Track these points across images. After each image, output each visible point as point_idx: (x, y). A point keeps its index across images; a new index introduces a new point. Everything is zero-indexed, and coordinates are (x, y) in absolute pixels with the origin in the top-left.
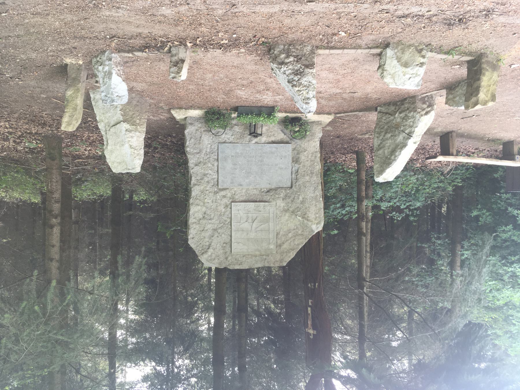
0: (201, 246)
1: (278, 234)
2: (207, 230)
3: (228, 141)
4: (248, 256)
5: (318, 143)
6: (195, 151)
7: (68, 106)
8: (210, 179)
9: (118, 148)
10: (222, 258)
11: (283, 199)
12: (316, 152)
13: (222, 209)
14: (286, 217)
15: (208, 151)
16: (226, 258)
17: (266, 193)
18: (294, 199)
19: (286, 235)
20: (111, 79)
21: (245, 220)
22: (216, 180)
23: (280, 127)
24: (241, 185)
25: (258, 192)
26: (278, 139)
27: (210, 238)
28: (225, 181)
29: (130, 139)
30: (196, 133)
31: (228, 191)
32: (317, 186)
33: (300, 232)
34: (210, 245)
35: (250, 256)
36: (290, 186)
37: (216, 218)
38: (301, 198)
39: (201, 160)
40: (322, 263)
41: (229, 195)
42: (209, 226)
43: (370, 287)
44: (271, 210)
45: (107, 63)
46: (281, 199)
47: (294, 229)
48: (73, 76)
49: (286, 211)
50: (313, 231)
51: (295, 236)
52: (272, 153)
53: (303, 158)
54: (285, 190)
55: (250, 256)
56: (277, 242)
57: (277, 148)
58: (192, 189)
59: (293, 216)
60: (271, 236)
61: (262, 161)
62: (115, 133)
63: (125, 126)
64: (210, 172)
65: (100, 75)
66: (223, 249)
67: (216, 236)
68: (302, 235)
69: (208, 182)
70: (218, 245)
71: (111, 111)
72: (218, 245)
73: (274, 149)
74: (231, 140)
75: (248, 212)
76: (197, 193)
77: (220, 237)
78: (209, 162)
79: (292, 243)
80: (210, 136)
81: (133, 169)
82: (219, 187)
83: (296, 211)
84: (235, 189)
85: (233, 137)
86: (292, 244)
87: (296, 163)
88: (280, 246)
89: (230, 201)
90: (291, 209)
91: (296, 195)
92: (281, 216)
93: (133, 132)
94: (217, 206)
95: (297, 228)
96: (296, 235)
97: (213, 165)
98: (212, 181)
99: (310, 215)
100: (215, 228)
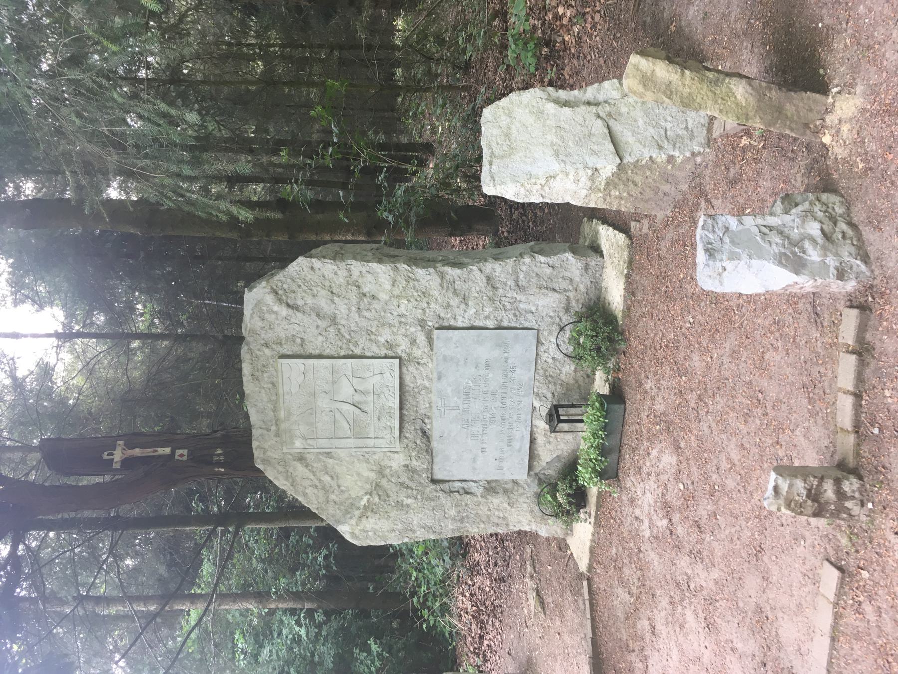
0: (295, 287)
2: (333, 301)
5: (527, 528)
6: (521, 276)
7: (702, 81)
8: (456, 310)
9: (549, 137)
10: (269, 336)
11: (406, 466)
12: (507, 525)
13: (385, 335)
14: (366, 473)
15: (522, 306)
16: (267, 345)
18: (407, 487)
20: (780, 263)
22: (453, 322)
24: (439, 378)
25: (422, 412)
27: (313, 309)
29: (571, 177)
30: (563, 277)
31: (427, 350)
33: (333, 497)
35: (274, 398)
37: (364, 323)
39: (501, 291)
41: (417, 353)
42: (342, 308)
43: (257, 38)
45: (831, 261)
46: (407, 462)
47: (339, 486)
48: (788, 106)
49: (381, 472)
51: (323, 488)
52: (510, 442)
53: (497, 501)
55: (274, 398)
58: (431, 270)
59: (368, 486)
60: (323, 443)
61: (493, 421)
62: (590, 134)
63: (608, 167)
65: (790, 220)
69: (448, 306)
71: (651, 131)
74: (544, 357)
75: (377, 394)
76: (423, 282)
77: (316, 332)
78: (496, 309)
79: (308, 483)
81: (493, 178)
82: (436, 331)
84: (430, 365)
85: (550, 361)
87: (485, 488)
89: (403, 355)
90: (384, 482)
92: (367, 461)
93: (589, 184)
94: (390, 325)
95: (342, 491)
96: (326, 490)
97: (487, 317)
98: (449, 315)
99: (372, 521)
100: (338, 320)
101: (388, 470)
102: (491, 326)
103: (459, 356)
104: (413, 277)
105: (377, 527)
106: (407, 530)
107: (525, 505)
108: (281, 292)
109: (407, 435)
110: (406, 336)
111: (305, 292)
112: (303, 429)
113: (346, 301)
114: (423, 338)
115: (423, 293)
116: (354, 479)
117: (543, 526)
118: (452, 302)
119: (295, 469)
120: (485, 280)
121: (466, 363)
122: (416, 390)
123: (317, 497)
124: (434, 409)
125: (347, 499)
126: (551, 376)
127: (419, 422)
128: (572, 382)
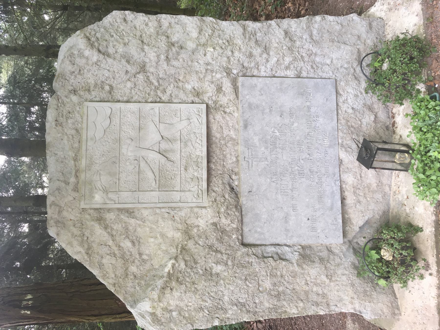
0: (107, 37)
1: (130, 212)
2: (143, 50)
3: (341, 100)
4: (76, 140)
6: (315, 32)
11: (215, 224)
14: (171, 234)
15: (318, 59)
16: (75, 92)
17: (230, 185)
18: (217, 251)
19: (127, 233)
21: (165, 134)
22: (255, 73)
23: (377, 217)
24: (246, 126)
26: (350, 211)
28: (254, 91)
32: (248, 312)
33: (133, 269)
34: (109, 56)
35: (76, 145)
36: (245, 241)
38: (218, 269)
39: (298, 43)
40: (74, 322)
41: (223, 100)
42: (151, 55)
44: (188, 196)
46: (216, 220)
47: (140, 254)
49: (187, 233)
50: (135, 303)
52: (320, 198)
53: (314, 271)
54: (237, 229)
56: (109, 210)
57: (331, 209)
59: (173, 251)
60: (125, 196)
61: (301, 174)
64: (274, 60)
66: (96, 85)
67: (129, 68)
68: (127, 275)
69: (251, 55)
70: (107, 74)
72: (107, 74)
73: (328, 202)
75: (185, 143)
77: (125, 78)
78: (295, 59)
80: (348, 63)
82: (241, 79)
83: (187, 258)
84: (236, 114)
85: (350, 111)
86: (104, 250)
87: (300, 254)
88: (100, 220)
89: (210, 102)
90: (190, 244)
91: (225, 257)
92: (173, 219)
94: (197, 72)
95: (144, 261)
96: (126, 259)
98: (253, 65)
99: (176, 294)
100: (147, 68)
101: (195, 230)
102: (292, 76)
103: (264, 104)
104: (218, 28)
105: (182, 304)
106: (217, 308)
107: (344, 278)
108: (93, 39)
109: (216, 189)
110: (212, 82)
111: (117, 41)
112: (104, 180)
113: (156, 50)
114: (229, 85)
115: (228, 41)
116: (157, 243)
117: (367, 304)
118: (255, 52)
119: (92, 233)
120: (283, 33)
121: (271, 111)
122: (223, 142)
123: (115, 267)
124: (242, 162)
125: (149, 271)
126: (352, 127)
127: (226, 177)
128: (373, 133)
